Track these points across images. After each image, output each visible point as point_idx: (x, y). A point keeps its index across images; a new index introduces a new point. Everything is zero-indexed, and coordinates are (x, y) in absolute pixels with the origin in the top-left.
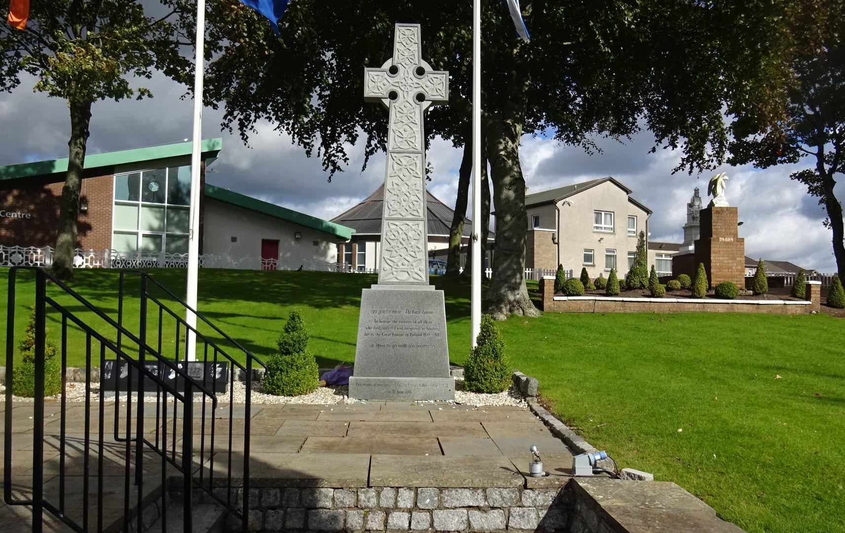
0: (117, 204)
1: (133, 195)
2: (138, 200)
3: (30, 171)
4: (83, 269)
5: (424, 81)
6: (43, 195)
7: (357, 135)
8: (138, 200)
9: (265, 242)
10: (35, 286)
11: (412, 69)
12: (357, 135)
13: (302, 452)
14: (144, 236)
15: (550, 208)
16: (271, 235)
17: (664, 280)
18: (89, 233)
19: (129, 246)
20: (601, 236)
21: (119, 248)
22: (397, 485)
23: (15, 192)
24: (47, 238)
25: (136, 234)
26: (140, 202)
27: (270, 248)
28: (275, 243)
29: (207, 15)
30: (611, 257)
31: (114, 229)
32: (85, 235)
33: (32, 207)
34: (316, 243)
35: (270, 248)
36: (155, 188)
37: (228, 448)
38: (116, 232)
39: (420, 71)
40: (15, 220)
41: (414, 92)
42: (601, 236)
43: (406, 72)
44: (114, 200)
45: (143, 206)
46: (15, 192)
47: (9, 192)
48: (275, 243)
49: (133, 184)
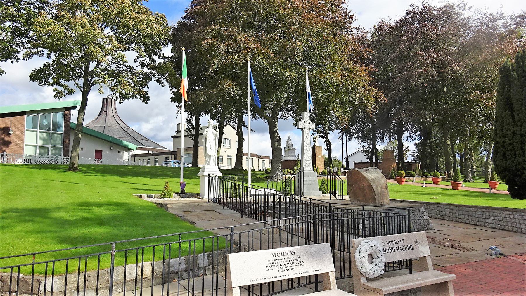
0: (27, 130)
1: (35, 127)
2: (37, 128)
5: (310, 125)
8: (37, 128)
9: (96, 151)
11: (308, 122)
15: (179, 138)
16: (99, 149)
18: (10, 146)
20: (226, 150)
21: (29, 152)
26: (39, 130)
27: (98, 154)
28: (100, 152)
29: (247, 104)
30: (229, 158)
31: (25, 143)
34: (119, 152)
35: (98, 154)
37: (144, 263)
38: (26, 145)
39: (309, 123)
41: (306, 123)
42: (226, 150)
43: (307, 122)
44: (26, 129)
48: (100, 152)
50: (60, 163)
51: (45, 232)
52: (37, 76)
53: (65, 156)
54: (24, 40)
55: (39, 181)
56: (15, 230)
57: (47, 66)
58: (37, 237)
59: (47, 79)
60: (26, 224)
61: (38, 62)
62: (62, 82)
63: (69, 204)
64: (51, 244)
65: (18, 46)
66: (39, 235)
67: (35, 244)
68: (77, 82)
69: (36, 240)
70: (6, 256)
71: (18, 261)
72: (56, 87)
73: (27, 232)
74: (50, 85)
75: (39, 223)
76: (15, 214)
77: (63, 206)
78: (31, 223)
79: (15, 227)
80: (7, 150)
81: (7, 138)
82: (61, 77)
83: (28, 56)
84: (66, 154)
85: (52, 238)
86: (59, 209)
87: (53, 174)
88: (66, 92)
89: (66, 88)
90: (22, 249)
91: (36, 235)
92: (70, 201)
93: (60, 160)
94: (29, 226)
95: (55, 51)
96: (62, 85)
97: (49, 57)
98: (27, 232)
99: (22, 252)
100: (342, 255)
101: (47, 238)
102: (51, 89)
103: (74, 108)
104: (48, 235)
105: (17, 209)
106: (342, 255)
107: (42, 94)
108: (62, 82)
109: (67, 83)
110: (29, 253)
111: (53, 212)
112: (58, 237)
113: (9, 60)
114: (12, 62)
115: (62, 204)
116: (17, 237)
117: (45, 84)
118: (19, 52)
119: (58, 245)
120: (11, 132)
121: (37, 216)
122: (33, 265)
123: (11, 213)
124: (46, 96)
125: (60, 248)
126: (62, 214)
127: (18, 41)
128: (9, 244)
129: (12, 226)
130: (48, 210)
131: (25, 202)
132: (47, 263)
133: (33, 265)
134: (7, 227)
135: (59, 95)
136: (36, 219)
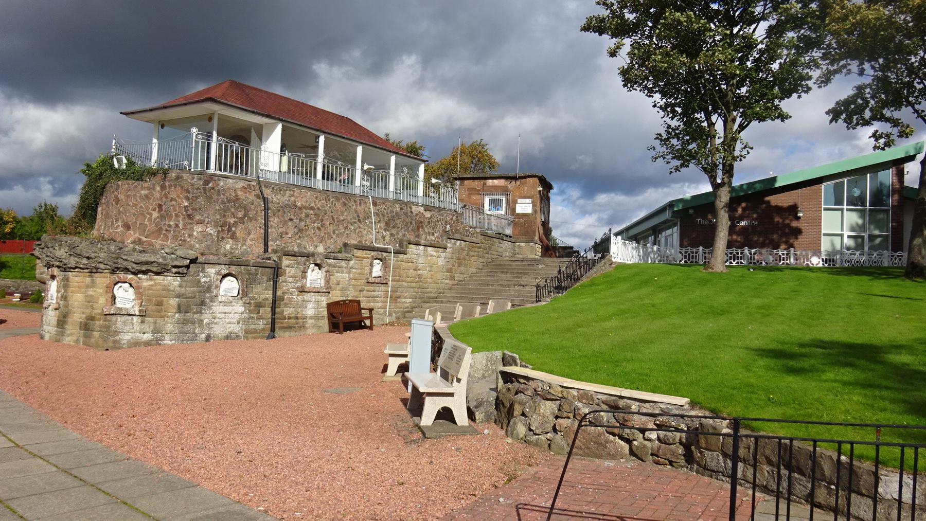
1: (839, 201)
3: (758, 187)
4: (866, 267)
6: (764, 206)
7: (625, 86)
8: (842, 204)
10: (629, 261)
12: (625, 86)
13: (278, 333)
14: (849, 237)
17: (514, 209)
19: (833, 245)
22: (840, 439)
23: (744, 205)
24: (767, 242)
25: (841, 236)
26: (845, 207)
31: (823, 232)
32: (797, 238)
33: (755, 216)
36: (857, 192)
38: (825, 235)
40: (743, 227)
45: (848, 210)
46: (744, 205)
47: (739, 205)
49: (838, 189)
50: (886, 264)
51: (880, 387)
52: (848, 113)
53: (895, 250)
54: (817, 54)
55: (851, 296)
56: (824, 377)
57: (860, 89)
58: (865, 396)
59: (861, 114)
60: (842, 370)
61: (843, 88)
62: (887, 113)
63: (915, 340)
64: (892, 411)
65: (809, 67)
66: (868, 392)
67: (862, 406)
68: (917, 107)
69: (864, 401)
70: (815, 420)
71: (850, 434)
72: (877, 126)
73: (845, 383)
74: (867, 123)
75: (864, 370)
76: (820, 350)
77: (904, 343)
78: (849, 369)
79: (823, 372)
80: (796, 243)
81: (794, 224)
82: (885, 104)
83: (826, 80)
84: (897, 245)
85: (893, 401)
86: (898, 348)
87: (880, 286)
88: (895, 131)
89: (895, 123)
90: (841, 413)
91: (863, 392)
92: (917, 335)
93: (886, 258)
94: (848, 374)
95: (872, 58)
96: (888, 120)
97: (861, 73)
98: (845, 383)
99: (841, 418)
100: (560, 512)
101: (883, 398)
102: (870, 130)
103: (911, 158)
104: (885, 393)
105: (822, 341)
106: (560, 512)
107: (857, 142)
108: (887, 113)
109: (896, 115)
110: (853, 421)
111: (887, 353)
112: (904, 401)
113: (795, 95)
114: (799, 97)
115: (902, 339)
116: (829, 390)
117: (857, 124)
118: (810, 78)
119: (910, 417)
120: (800, 215)
121: (858, 358)
122: (878, 446)
123: (814, 349)
124: (862, 145)
125: (911, 423)
126: (904, 358)
127: (807, 58)
128: (818, 400)
129: (817, 371)
130: (881, 347)
131: (836, 330)
132: (903, 446)
133: (878, 446)
134: (811, 371)
135: (884, 141)
136: (858, 362)
